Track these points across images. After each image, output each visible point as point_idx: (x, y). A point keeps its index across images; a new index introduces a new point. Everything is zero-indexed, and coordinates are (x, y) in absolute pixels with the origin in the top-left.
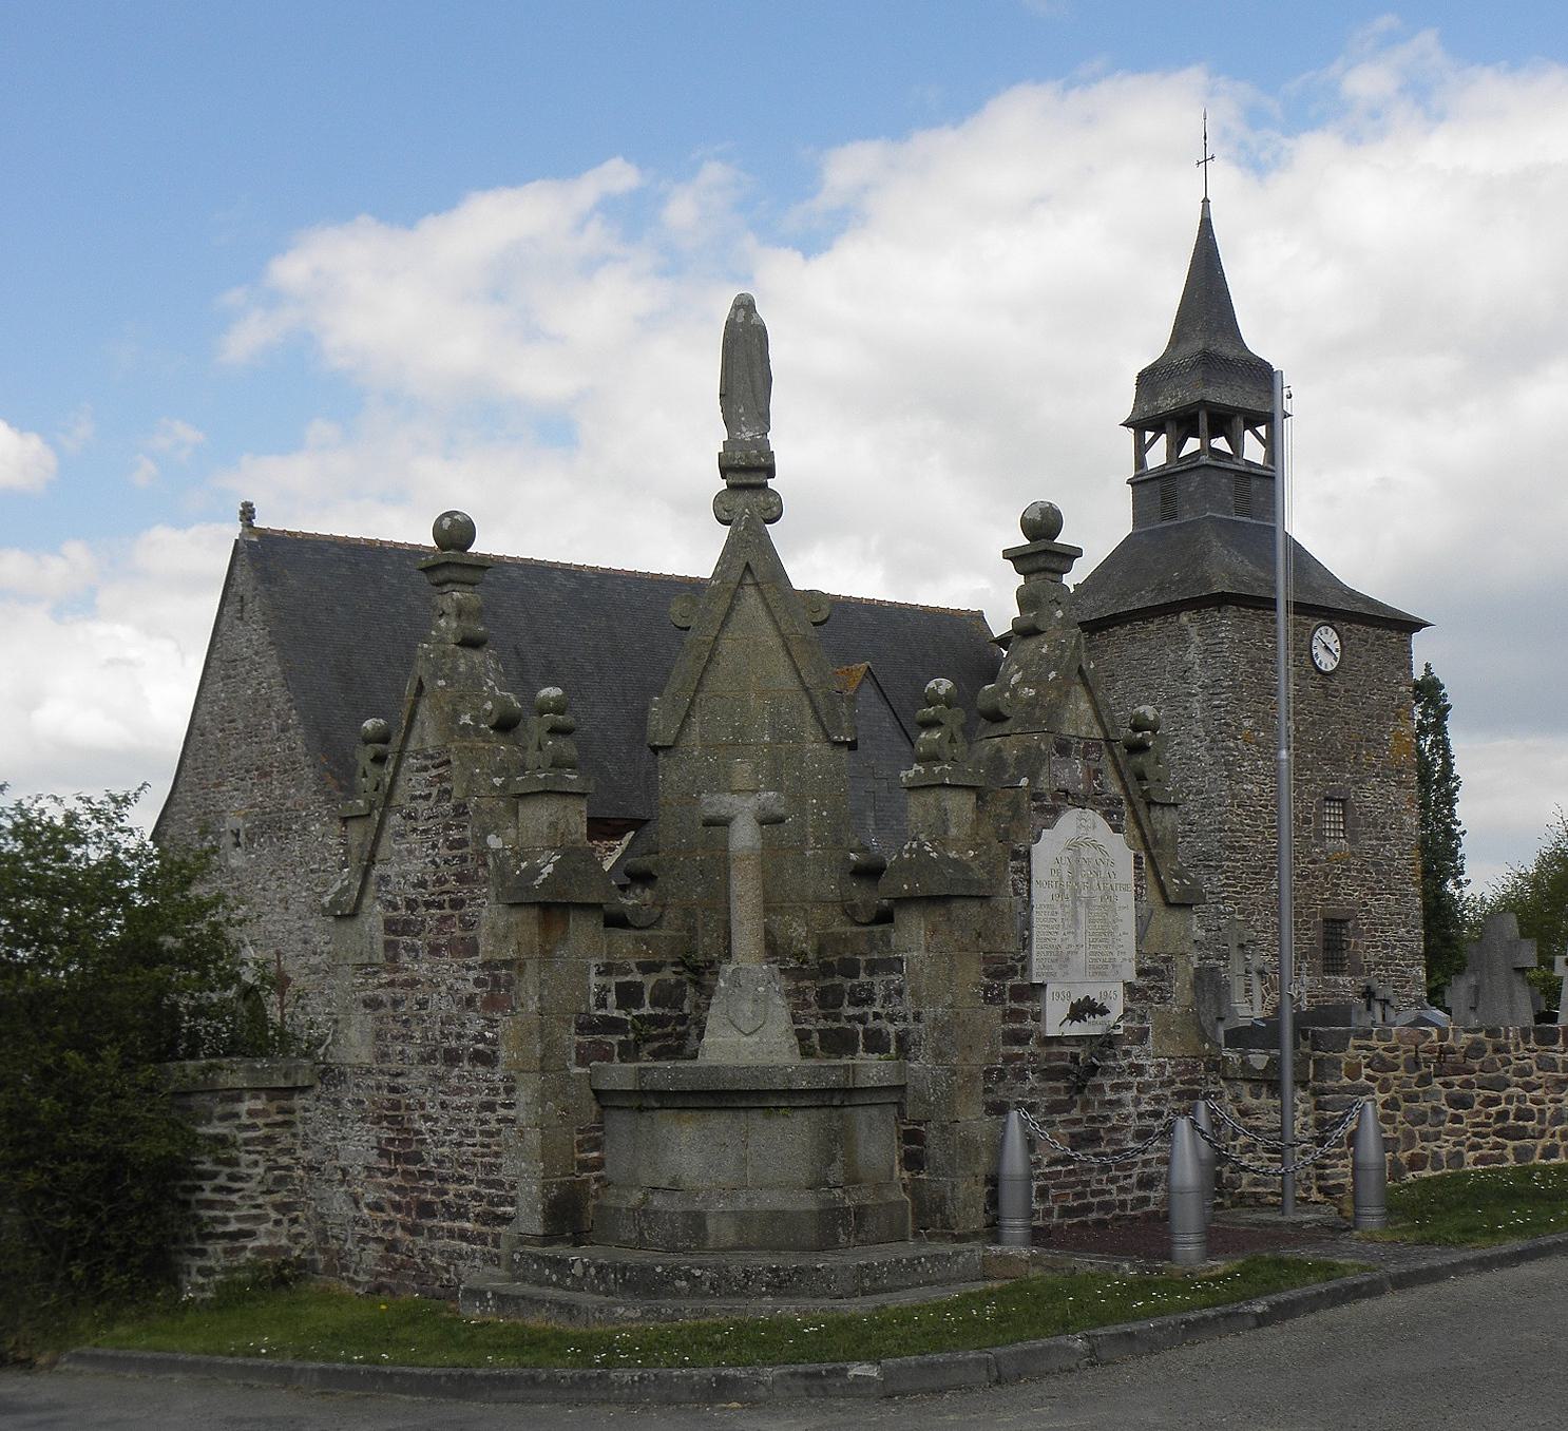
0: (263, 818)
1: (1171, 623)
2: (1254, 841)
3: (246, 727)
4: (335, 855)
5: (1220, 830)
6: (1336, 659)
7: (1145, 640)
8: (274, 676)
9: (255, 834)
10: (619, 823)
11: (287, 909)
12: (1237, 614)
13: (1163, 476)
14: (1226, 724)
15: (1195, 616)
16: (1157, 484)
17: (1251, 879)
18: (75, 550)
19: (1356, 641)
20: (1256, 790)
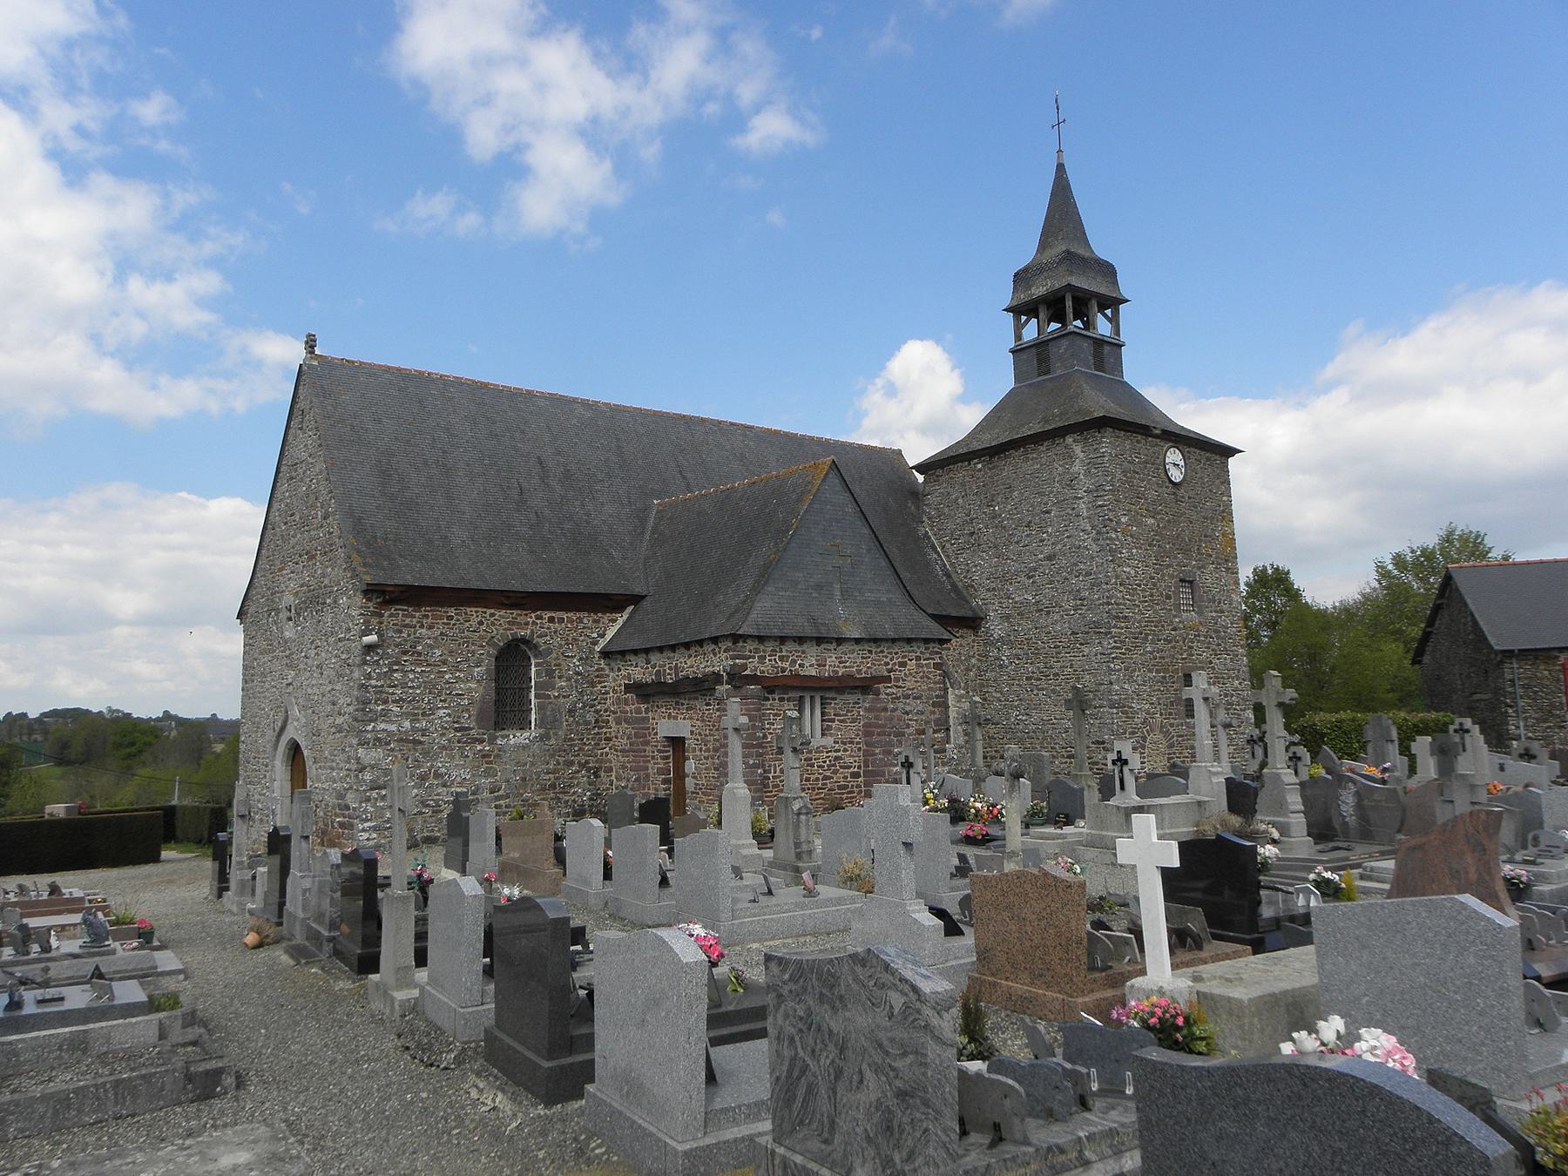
0: (307, 595)
1: (1058, 444)
2: (1133, 613)
3: (301, 518)
4: (357, 625)
5: (1109, 604)
6: (1182, 473)
7: (1037, 459)
8: (321, 473)
9: (301, 609)
10: (621, 598)
11: (322, 674)
12: (1113, 435)
13: (1041, 346)
14: (1109, 519)
15: (1079, 437)
16: (1034, 350)
17: (1132, 643)
18: (1393, 1039)
19: (1193, 461)
20: (1132, 572)
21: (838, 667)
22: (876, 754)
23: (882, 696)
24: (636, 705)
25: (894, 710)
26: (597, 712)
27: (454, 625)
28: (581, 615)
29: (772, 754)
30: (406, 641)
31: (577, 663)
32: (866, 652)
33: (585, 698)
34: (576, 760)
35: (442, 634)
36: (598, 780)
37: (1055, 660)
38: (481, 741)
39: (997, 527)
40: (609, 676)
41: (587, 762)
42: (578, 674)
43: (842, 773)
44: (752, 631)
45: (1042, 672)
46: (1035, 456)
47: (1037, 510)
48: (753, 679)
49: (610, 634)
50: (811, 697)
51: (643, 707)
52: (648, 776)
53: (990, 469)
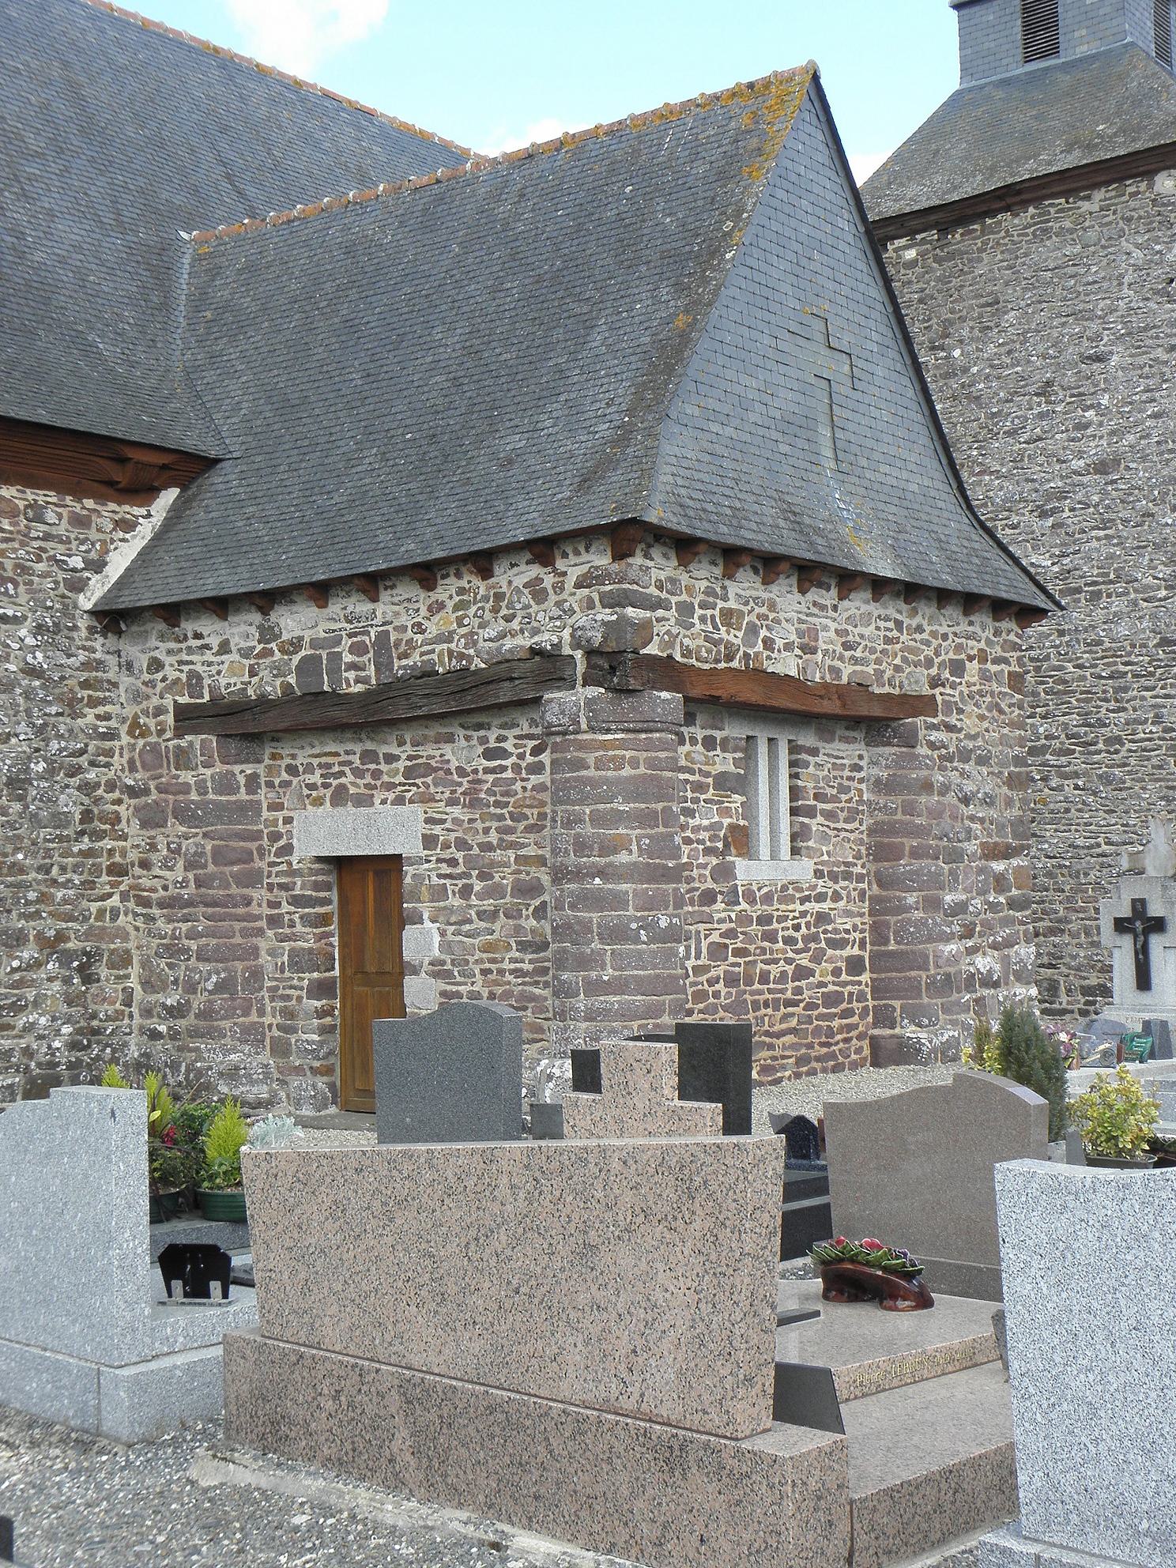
1: (1132, 195)
21: (841, 658)
22: (907, 909)
23: (922, 750)
24: (219, 768)
25: (945, 790)
26: (87, 788)
28: (40, 496)
29: (692, 904)
31: (30, 641)
32: (891, 625)
33: (54, 745)
34: (31, 927)
36: (94, 989)
37: (1112, 705)
39: (954, 398)
40: (115, 685)
41: (61, 937)
42: (32, 672)
43: (830, 960)
44: (675, 520)
45: (1074, 736)
46: (1068, 224)
47: (1071, 353)
48: (667, 672)
49: (119, 562)
50: (770, 740)
51: (241, 771)
52: (257, 974)
53: (938, 260)
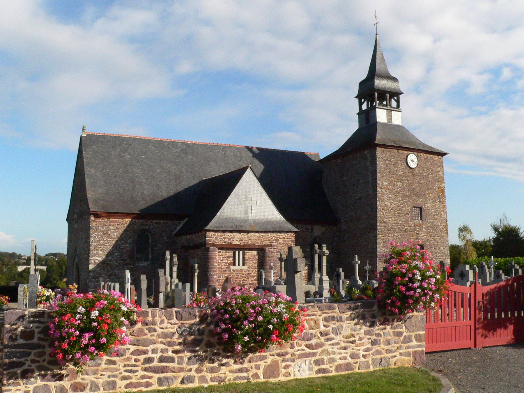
19: (423, 159)
27: (121, 225)
30: (105, 230)
35: (117, 228)
38: (130, 264)
